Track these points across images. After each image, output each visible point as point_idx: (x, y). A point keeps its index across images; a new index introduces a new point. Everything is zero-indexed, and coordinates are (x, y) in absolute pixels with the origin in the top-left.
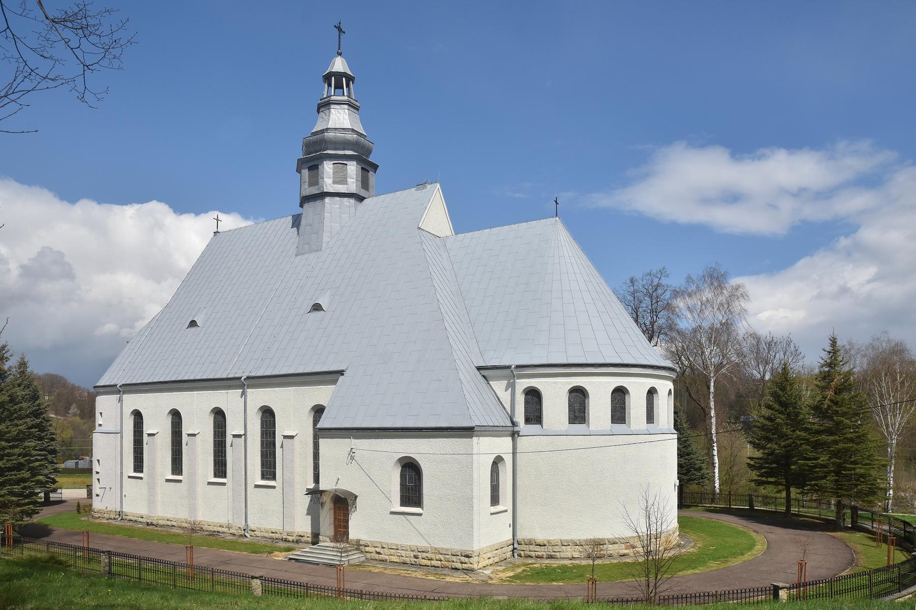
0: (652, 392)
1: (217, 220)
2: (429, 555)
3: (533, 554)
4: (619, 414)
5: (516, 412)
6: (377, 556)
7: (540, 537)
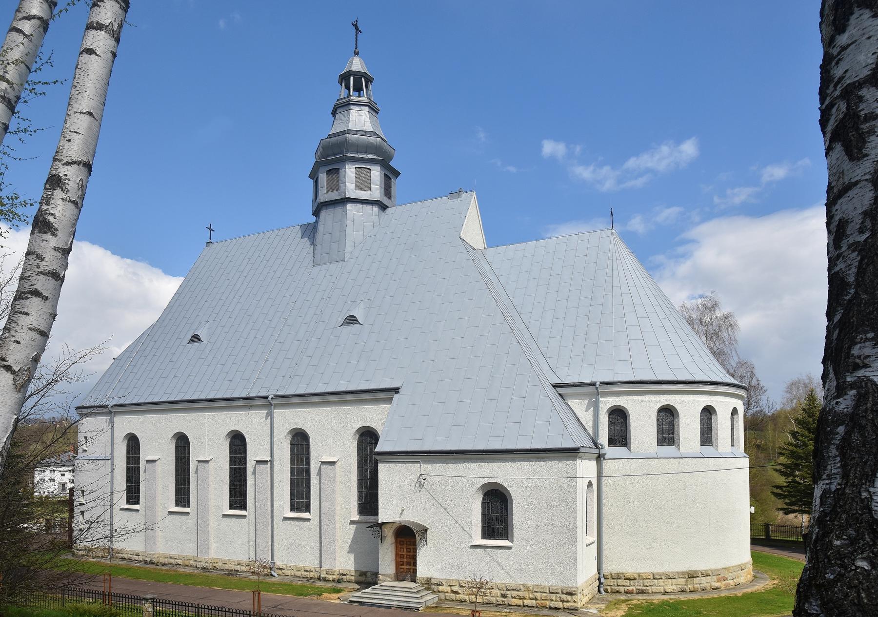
0: (708, 412)
1: (210, 229)
2: (521, 594)
3: (621, 589)
4: (707, 437)
5: (600, 433)
6: (453, 596)
7: (630, 570)
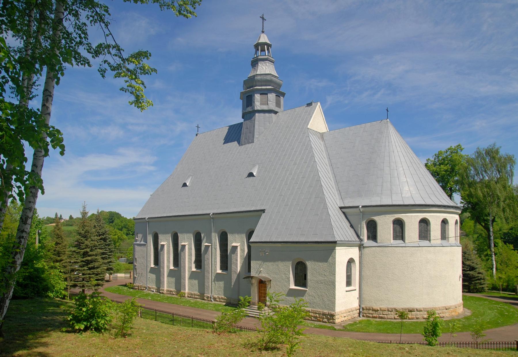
0: (445, 222)
1: (198, 127)
4: (444, 236)
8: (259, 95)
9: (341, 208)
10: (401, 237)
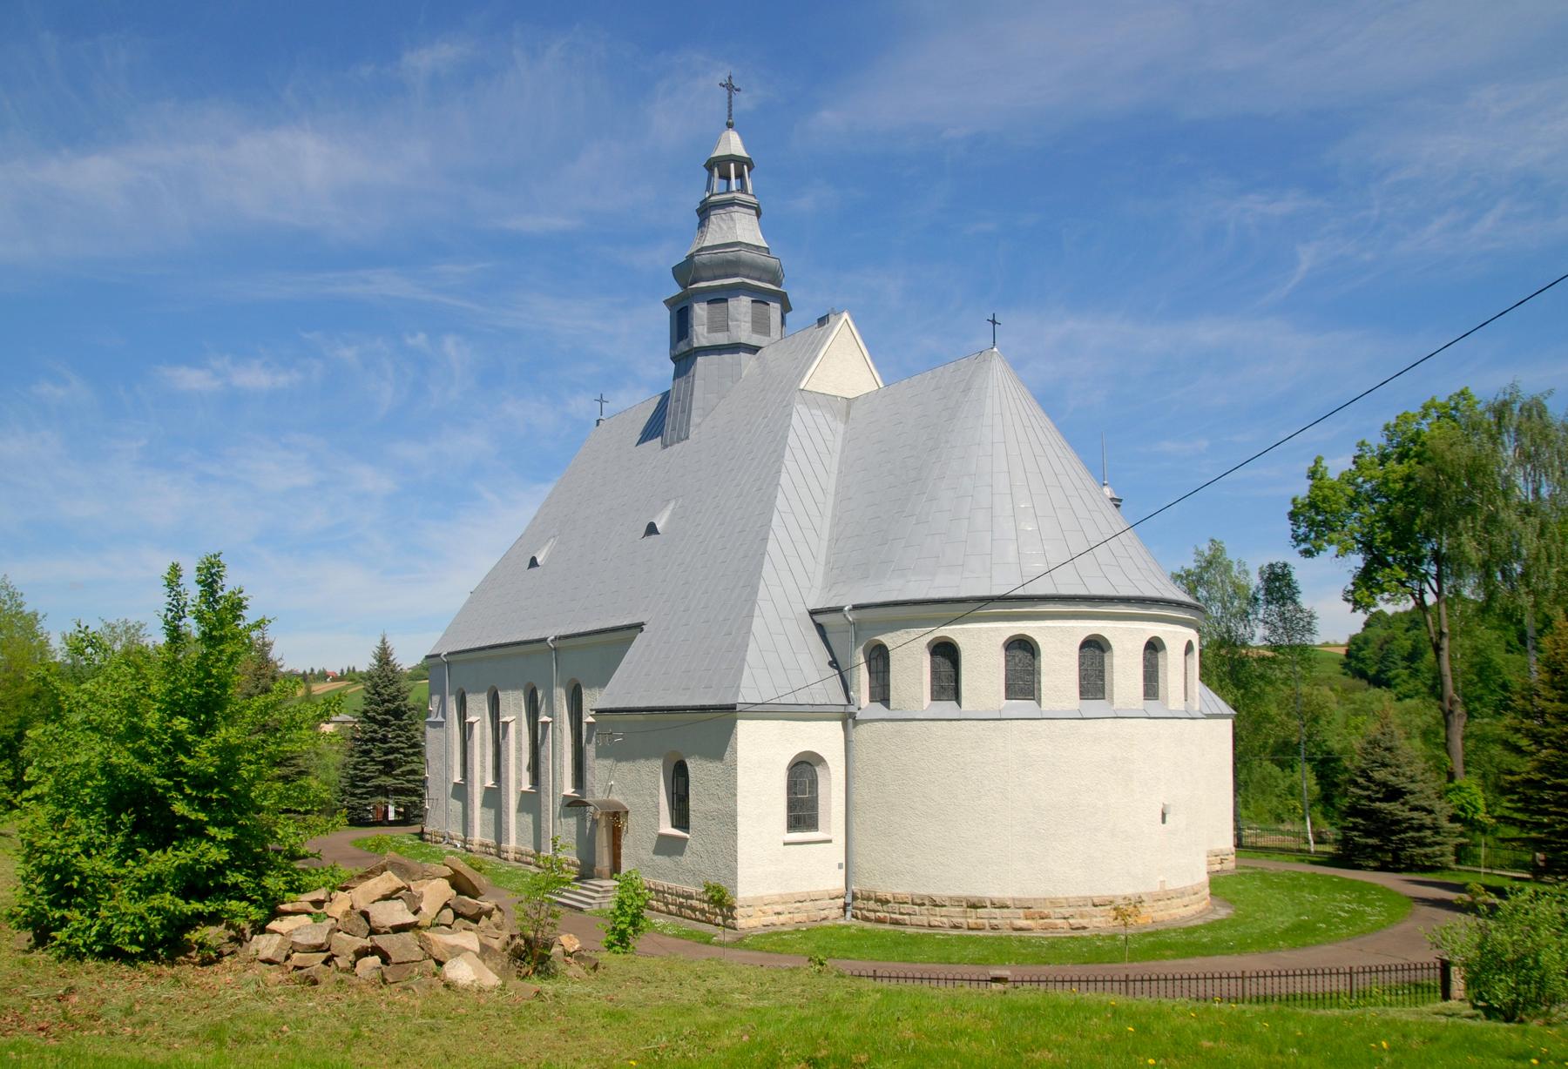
0: (1154, 647)
4: (1093, 682)
7: (884, 891)
8: (705, 305)
9: (813, 613)
10: (951, 692)
